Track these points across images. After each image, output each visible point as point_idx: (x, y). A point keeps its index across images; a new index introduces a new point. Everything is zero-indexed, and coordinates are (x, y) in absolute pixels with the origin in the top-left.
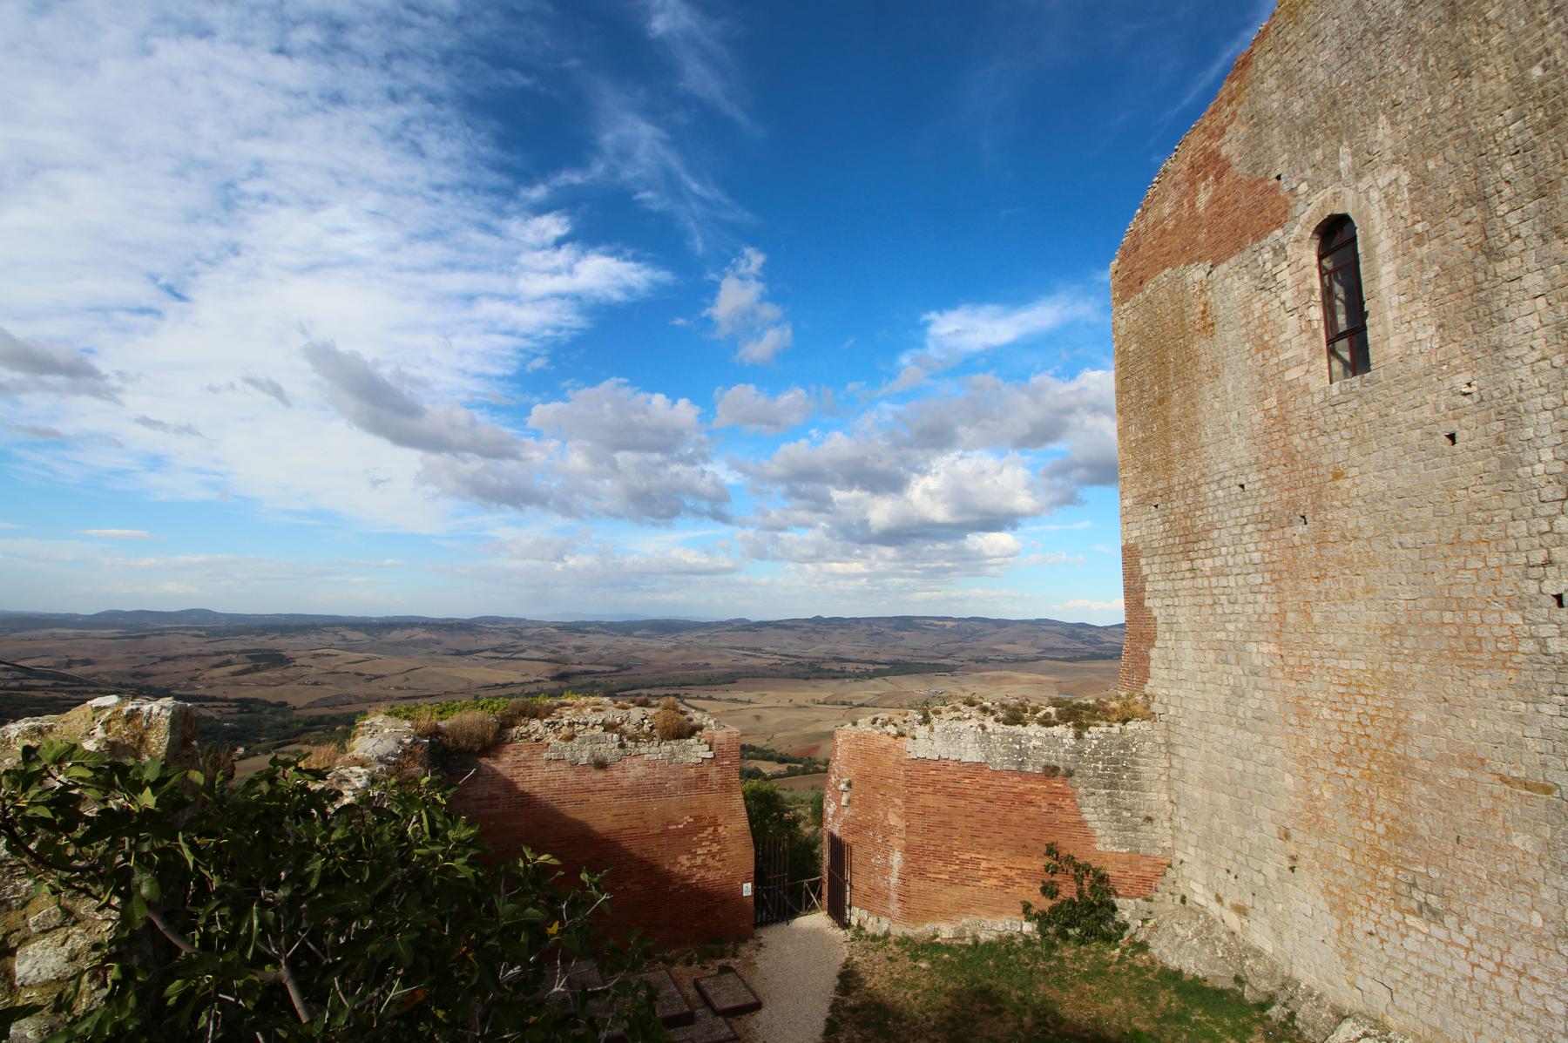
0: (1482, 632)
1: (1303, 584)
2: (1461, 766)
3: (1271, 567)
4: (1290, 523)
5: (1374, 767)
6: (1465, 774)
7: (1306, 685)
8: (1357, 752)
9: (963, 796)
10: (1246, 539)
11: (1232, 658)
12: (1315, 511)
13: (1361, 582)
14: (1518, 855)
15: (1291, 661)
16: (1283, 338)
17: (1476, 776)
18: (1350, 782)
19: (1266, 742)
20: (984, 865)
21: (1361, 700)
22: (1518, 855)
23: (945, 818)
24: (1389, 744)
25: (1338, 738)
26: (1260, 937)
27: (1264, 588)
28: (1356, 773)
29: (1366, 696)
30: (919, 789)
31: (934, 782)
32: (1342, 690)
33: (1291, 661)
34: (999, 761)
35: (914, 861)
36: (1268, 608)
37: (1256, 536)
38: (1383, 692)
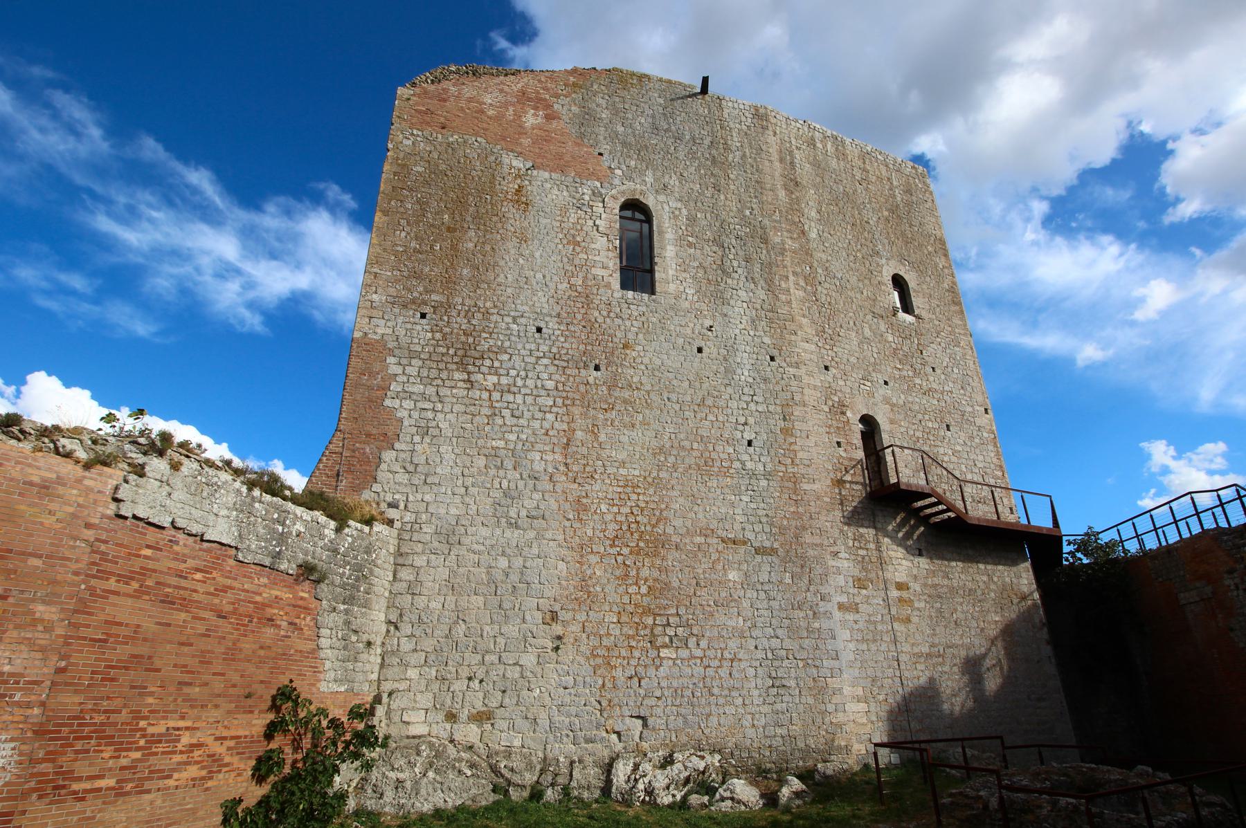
0: (714, 455)
1: (592, 412)
2: (700, 535)
3: (564, 394)
4: (586, 366)
5: (642, 544)
6: (702, 540)
7: (588, 487)
8: (628, 535)
9: (185, 604)
10: (539, 368)
11: (509, 464)
12: (608, 365)
13: (640, 417)
14: (731, 584)
15: (575, 468)
16: (593, 246)
17: (709, 540)
18: (620, 559)
19: (539, 536)
20: (186, 739)
21: (634, 497)
22: (731, 584)
23: (143, 650)
24: (654, 526)
25: (612, 526)
26: (510, 736)
27: (555, 410)
28: (626, 551)
29: (639, 494)
30: (112, 584)
31: (144, 572)
32: (619, 490)
33: (575, 468)
34: (255, 548)
35: (51, 757)
36: (556, 425)
37: (552, 369)
38: (651, 491)
